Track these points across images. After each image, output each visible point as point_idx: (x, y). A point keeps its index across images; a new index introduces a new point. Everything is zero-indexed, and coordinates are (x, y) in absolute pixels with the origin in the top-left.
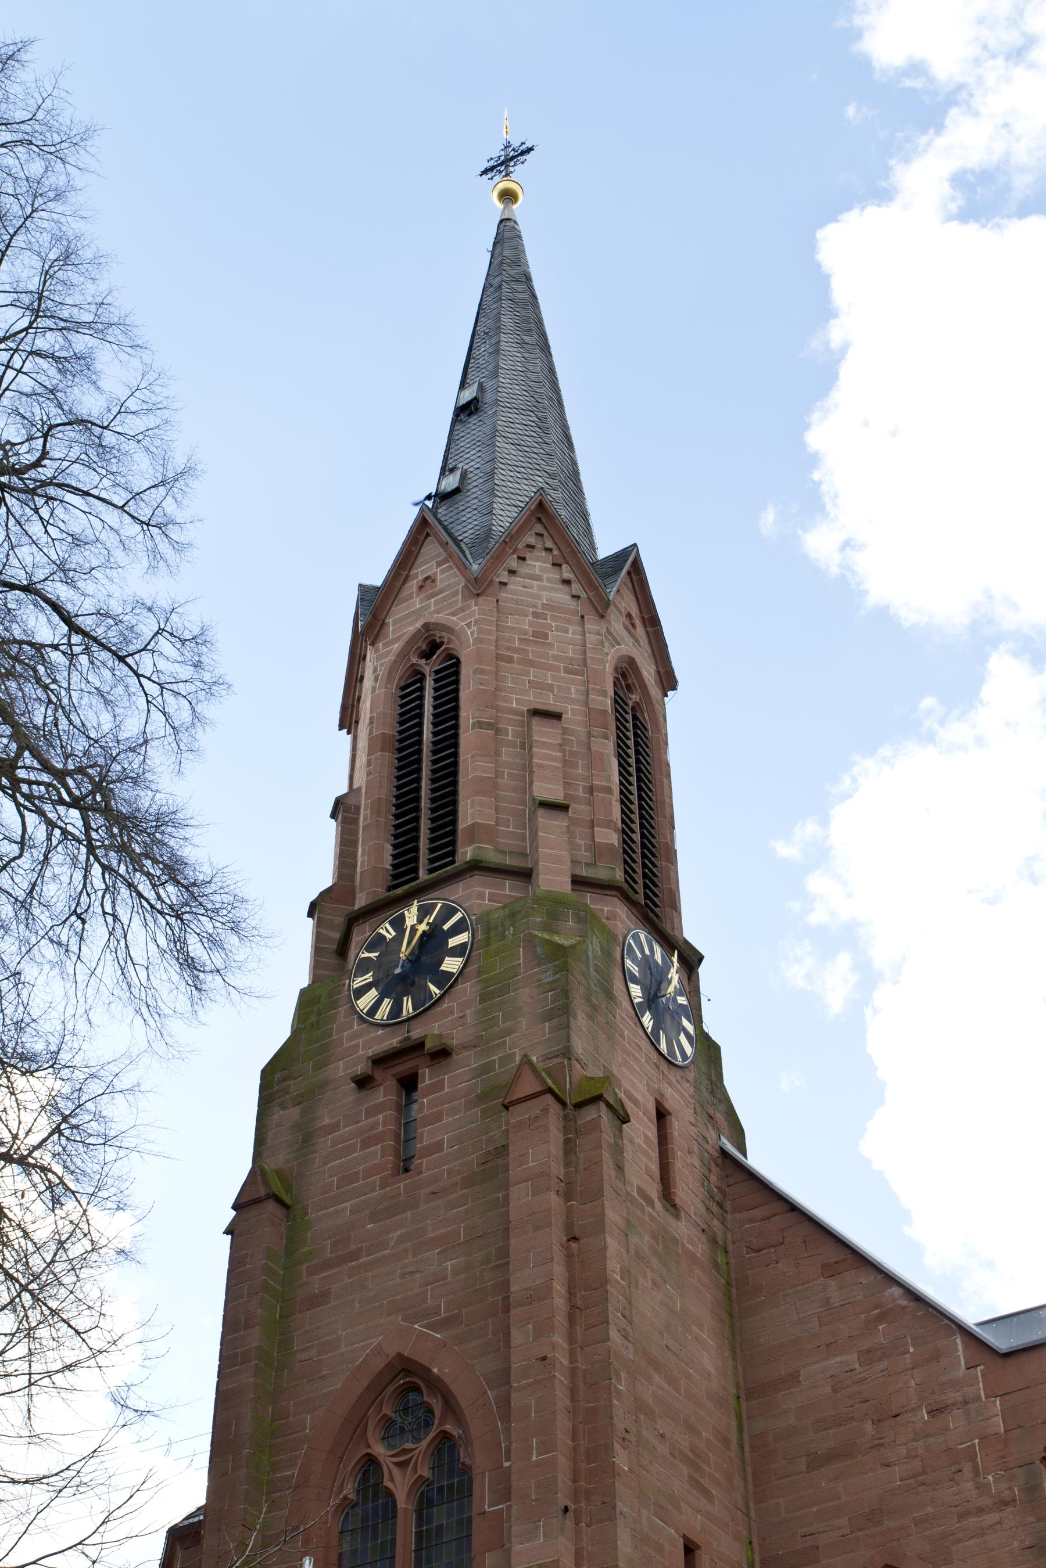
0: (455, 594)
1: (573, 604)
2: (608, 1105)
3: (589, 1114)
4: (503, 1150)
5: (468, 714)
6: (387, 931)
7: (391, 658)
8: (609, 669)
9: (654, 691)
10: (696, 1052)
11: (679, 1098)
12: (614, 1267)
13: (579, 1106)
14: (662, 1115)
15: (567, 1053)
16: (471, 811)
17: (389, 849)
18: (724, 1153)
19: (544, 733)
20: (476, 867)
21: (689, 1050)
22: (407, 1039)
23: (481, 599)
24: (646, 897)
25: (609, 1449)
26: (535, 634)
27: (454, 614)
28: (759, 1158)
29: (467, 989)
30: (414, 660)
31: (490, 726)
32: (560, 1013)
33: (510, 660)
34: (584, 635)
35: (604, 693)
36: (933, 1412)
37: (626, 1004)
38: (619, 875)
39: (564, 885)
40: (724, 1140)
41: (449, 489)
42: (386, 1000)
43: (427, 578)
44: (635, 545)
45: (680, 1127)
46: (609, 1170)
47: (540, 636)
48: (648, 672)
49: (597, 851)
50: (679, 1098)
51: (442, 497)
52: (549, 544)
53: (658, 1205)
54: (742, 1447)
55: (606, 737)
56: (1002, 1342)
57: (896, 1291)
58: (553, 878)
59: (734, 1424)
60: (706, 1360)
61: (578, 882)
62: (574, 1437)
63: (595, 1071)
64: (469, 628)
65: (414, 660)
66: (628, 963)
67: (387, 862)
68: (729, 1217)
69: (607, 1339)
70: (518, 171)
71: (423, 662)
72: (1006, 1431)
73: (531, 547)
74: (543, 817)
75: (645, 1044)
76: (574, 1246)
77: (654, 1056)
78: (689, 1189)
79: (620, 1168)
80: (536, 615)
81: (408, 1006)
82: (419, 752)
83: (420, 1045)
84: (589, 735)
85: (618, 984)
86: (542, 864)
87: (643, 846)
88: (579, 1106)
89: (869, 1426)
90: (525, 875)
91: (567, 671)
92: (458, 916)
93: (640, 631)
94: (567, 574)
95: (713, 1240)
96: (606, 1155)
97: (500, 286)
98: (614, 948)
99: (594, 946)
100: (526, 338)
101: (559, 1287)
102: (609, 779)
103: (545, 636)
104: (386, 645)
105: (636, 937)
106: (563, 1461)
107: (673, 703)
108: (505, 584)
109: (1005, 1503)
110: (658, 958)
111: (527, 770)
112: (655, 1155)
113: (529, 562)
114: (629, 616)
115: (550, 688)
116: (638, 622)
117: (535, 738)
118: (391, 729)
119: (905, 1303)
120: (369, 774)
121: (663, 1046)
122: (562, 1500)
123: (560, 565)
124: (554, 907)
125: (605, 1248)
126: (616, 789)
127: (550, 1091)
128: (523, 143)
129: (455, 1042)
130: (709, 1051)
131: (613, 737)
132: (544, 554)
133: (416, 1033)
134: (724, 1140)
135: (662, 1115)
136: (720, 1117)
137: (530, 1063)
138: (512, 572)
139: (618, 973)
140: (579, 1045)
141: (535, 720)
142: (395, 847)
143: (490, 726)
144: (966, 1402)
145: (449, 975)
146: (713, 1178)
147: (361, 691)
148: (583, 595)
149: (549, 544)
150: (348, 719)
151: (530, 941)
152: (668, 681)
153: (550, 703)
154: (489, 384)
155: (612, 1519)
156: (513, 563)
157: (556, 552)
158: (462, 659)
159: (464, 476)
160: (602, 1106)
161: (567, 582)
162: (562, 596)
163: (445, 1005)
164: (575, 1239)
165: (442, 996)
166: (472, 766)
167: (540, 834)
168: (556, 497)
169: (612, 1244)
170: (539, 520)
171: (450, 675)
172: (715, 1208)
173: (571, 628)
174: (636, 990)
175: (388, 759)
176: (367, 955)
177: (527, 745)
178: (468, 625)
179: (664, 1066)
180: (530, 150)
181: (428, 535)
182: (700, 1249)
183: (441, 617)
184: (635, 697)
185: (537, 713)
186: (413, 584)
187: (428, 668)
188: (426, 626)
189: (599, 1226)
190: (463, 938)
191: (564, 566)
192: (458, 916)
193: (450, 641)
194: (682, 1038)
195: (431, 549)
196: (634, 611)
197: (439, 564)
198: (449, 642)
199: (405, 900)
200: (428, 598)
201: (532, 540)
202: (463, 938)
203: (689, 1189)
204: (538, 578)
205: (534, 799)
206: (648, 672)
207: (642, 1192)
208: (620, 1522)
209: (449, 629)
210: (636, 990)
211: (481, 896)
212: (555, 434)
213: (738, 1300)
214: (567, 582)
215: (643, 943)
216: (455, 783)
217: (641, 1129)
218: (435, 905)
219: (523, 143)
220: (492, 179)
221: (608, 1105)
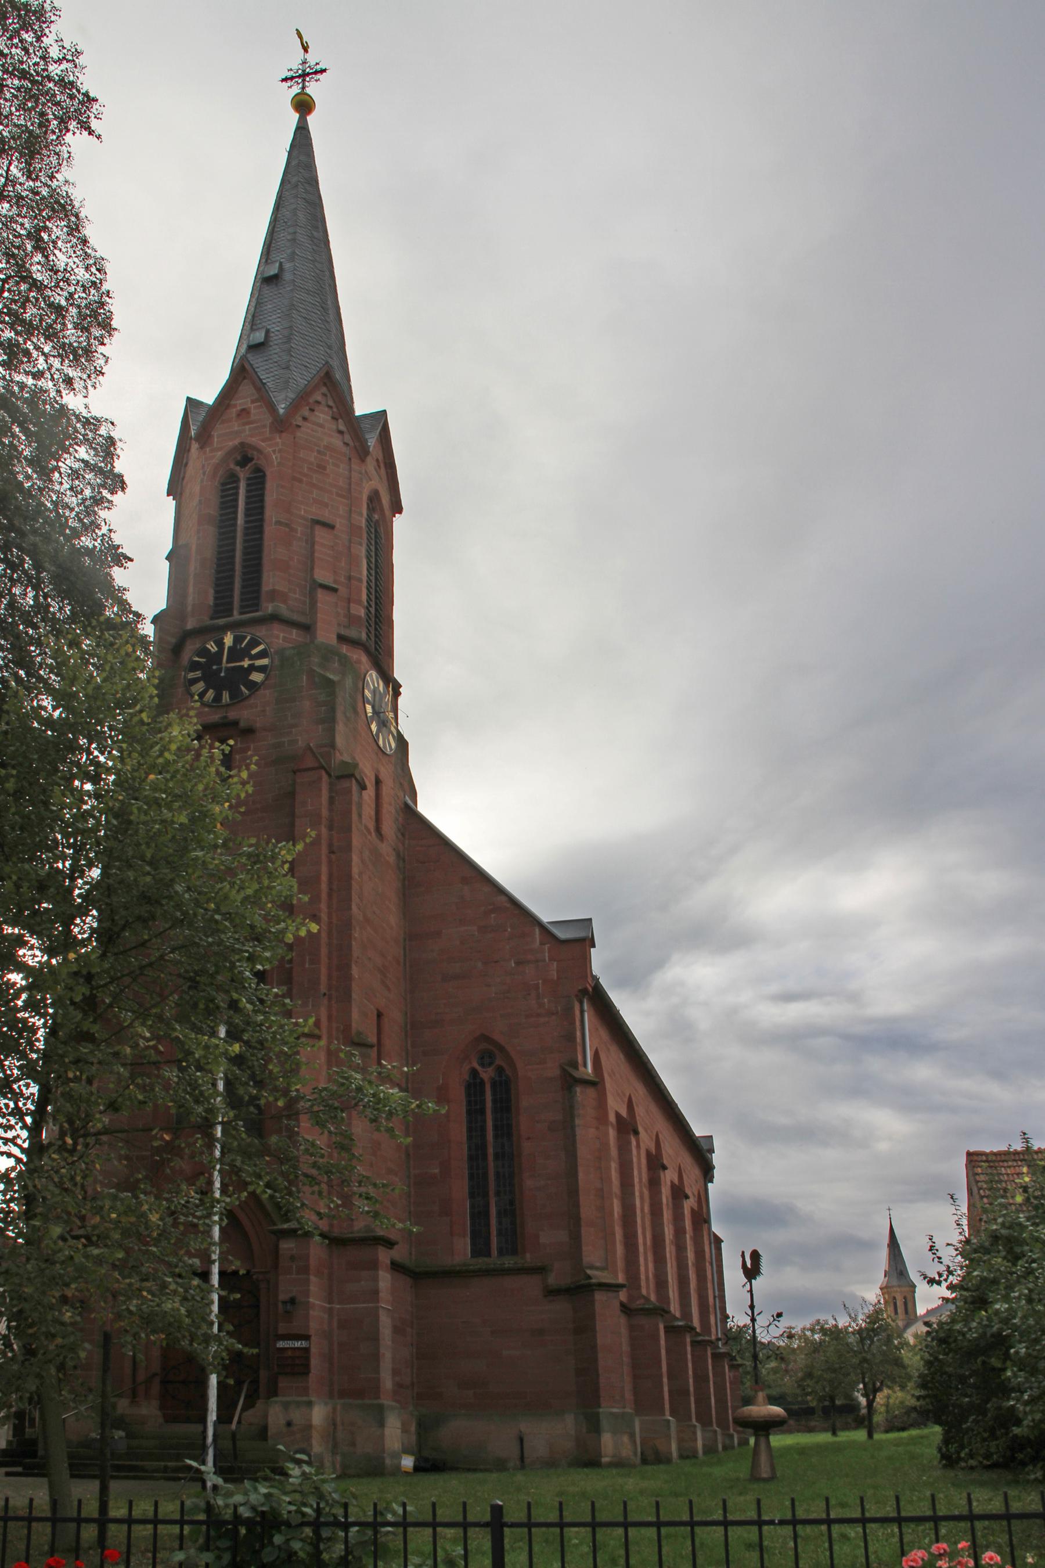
0: (264, 426)
1: (344, 449)
2: (356, 779)
3: (345, 784)
4: (292, 795)
5: (271, 514)
6: (212, 647)
7: (215, 461)
8: (365, 498)
9: (388, 512)
10: (397, 746)
11: (387, 773)
12: (355, 871)
13: (339, 778)
14: (378, 782)
15: (332, 745)
16: (271, 580)
17: (211, 592)
18: (406, 805)
19: (320, 533)
20: (275, 618)
21: (393, 745)
22: (226, 717)
23: (284, 434)
24: (376, 649)
25: (349, 967)
26: (319, 466)
27: (263, 441)
28: (423, 808)
29: (266, 694)
30: (232, 466)
31: (287, 525)
32: (329, 721)
33: (300, 481)
34: (350, 471)
35: (361, 515)
36: (518, 963)
37: (363, 717)
38: (364, 636)
39: (333, 641)
40: (407, 798)
41: (257, 342)
42: (211, 691)
43: (243, 410)
44: (385, 411)
45: (386, 790)
46: (355, 817)
47: (321, 467)
48: (385, 500)
49: (352, 620)
50: (387, 773)
51: (254, 348)
52: (331, 403)
53: (373, 834)
54: (405, 964)
55: (361, 544)
56: (562, 934)
57: (503, 898)
58: (326, 635)
59: (402, 952)
60: (392, 920)
61: (341, 638)
62: (329, 958)
63: (347, 758)
64: (273, 452)
65: (232, 466)
66: (366, 691)
67: (211, 601)
68: (407, 842)
69: (350, 909)
70: (295, 64)
71: (238, 468)
72: (558, 978)
73: (318, 403)
74: (320, 594)
75: (371, 740)
76: (333, 856)
77: (376, 747)
78: (389, 827)
79: (360, 816)
80: (319, 452)
81: (226, 697)
82: (235, 531)
83: (236, 723)
84: (350, 541)
85: (360, 704)
86: (319, 624)
87: (376, 617)
88: (339, 778)
89: (480, 965)
90: (307, 628)
91: (338, 495)
92: (261, 647)
93: (383, 471)
94: (342, 427)
95: (398, 855)
96: (354, 808)
97: (297, 186)
98: (360, 680)
99: (349, 682)
100: (315, 233)
101: (324, 878)
102: (361, 573)
103: (325, 468)
104: (212, 451)
105: (371, 675)
106: (324, 971)
107: (398, 521)
108: (299, 426)
109: (553, 1014)
110: (381, 689)
111: (310, 561)
112: (373, 806)
113: (317, 413)
114: (377, 460)
115: (326, 505)
116: (382, 465)
117: (317, 539)
118: (213, 510)
119: (508, 905)
120: (199, 538)
121: (381, 743)
122: (323, 988)
123: (337, 420)
124: (328, 654)
125: (351, 861)
126: (365, 579)
127: (323, 768)
128: (317, 64)
129: (258, 725)
130: (402, 744)
131: (365, 546)
132: (326, 409)
133: (232, 715)
134: (407, 798)
135: (378, 782)
136: (406, 784)
137: (310, 749)
138: (305, 419)
139: (360, 697)
140: (339, 741)
141: (317, 528)
142: (216, 592)
143: (287, 525)
144: (537, 961)
145: (254, 683)
146: (400, 819)
147: (185, 473)
148: (351, 444)
149: (331, 403)
150: (175, 488)
151: (311, 673)
152: (398, 508)
153: (326, 515)
154: (287, 266)
155: (350, 1002)
156: (305, 412)
157: (335, 410)
158: (268, 473)
159: (268, 332)
160: (354, 781)
161: (341, 432)
162: (337, 442)
163: (252, 701)
164: (333, 852)
165: (250, 696)
166: (273, 550)
167: (319, 605)
168: (335, 363)
169: (355, 859)
170: (325, 384)
171: (258, 481)
172: (400, 836)
173: (342, 466)
174: (369, 708)
175: (211, 531)
176: (197, 659)
177: (311, 543)
178: (274, 451)
179: (380, 753)
180: (323, 71)
181: (245, 378)
182: (392, 859)
183: (254, 441)
184: (376, 517)
185: (318, 522)
186: (233, 412)
187: (243, 474)
188: (242, 444)
189: (349, 848)
190: (265, 661)
191: (340, 421)
192: (261, 647)
193: (258, 459)
194: (391, 737)
195: (246, 390)
196: (381, 458)
197: (253, 402)
198: (258, 459)
199: (225, 629)
200: (244, 424)
201: (319, 398)
202: (265, 661)
203: (389, 827)
204: (321, 426)
205: (314, 581)
206: (385, 500)
207: (366, 827)
208: (353, 1002)
209: (260, 451)
210: (369, 708)
211: (278, 637)
212: (332, 317)
213: (410, 886)
214: (341, 432)
215: (373, 677)
216: (260, 558)
217: (369, 794)
218: (245, 637)
219: (317, 64)
220: (290, 87)
221: (356, 779)
